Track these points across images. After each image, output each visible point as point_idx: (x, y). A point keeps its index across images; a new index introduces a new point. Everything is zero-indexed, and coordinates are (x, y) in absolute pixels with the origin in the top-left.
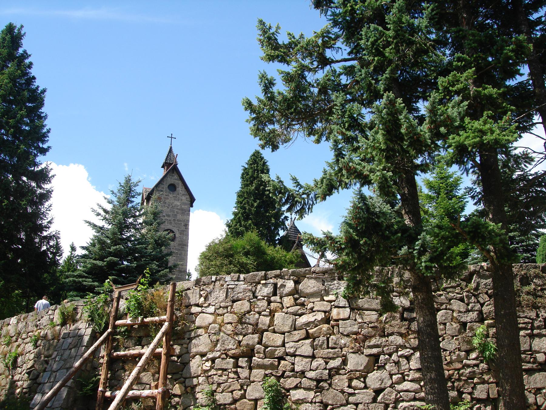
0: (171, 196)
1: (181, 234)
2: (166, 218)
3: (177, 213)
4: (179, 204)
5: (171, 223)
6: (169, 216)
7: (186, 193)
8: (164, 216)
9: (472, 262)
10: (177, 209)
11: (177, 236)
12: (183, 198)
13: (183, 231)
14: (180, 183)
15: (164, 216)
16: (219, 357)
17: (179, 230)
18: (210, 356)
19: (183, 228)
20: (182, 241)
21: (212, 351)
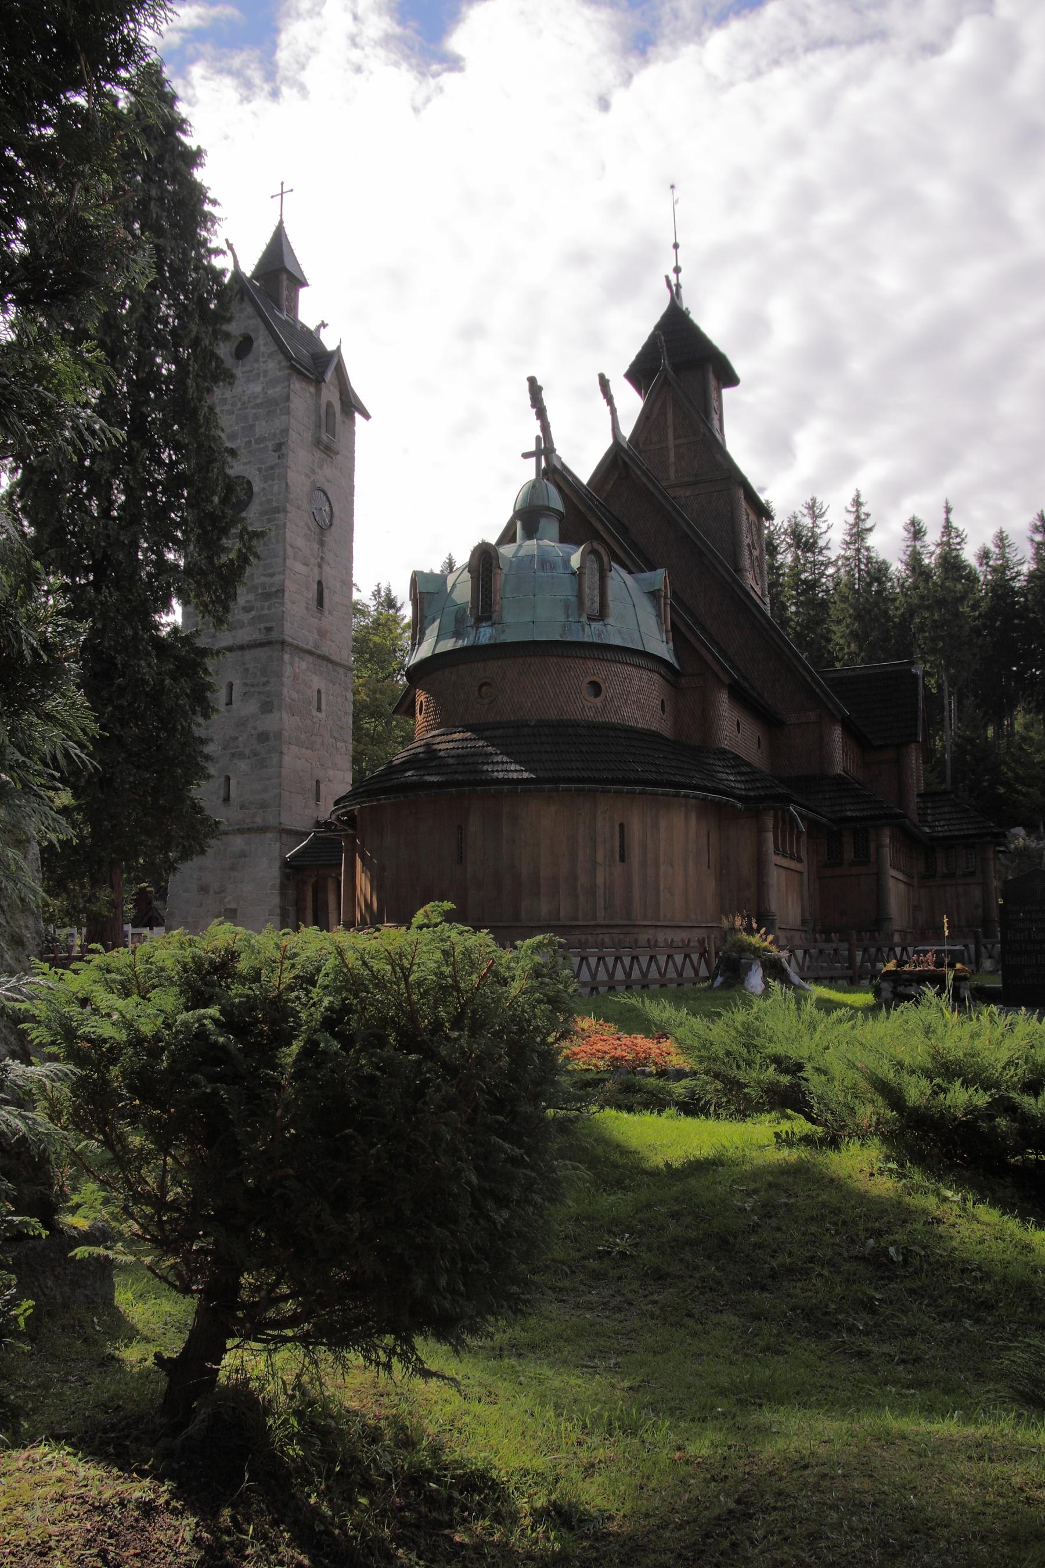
1: (265, 479)
3: (256, 418)
9: (252, 689)
12: (272, 365)
14: (263, 331)
17: (260, 470)
19: (272, 458)
20: (269, 501)
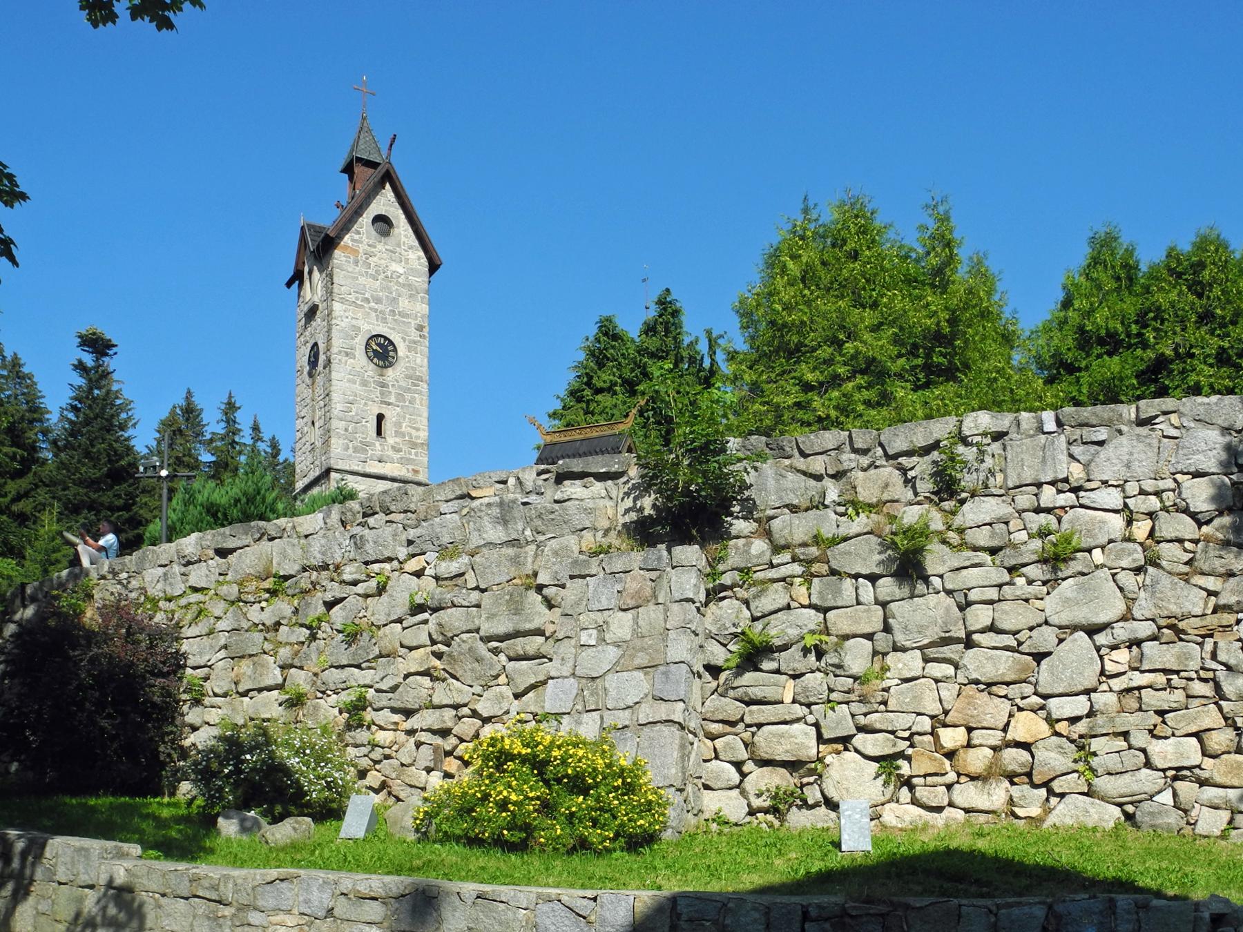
0: (380, 247)
1: (409, 349)
2: (372, 304)
4: (401, 271)
5: (384, 320)
6: (378, 300)
7: (416, 243)
8: (367, 300)
10: (398, 283)
11: (400, 353)
13: (415, 342)
15: (367, 300)
16: (1154, 638)
18: (1122, 632)
21: (1127, 617)
